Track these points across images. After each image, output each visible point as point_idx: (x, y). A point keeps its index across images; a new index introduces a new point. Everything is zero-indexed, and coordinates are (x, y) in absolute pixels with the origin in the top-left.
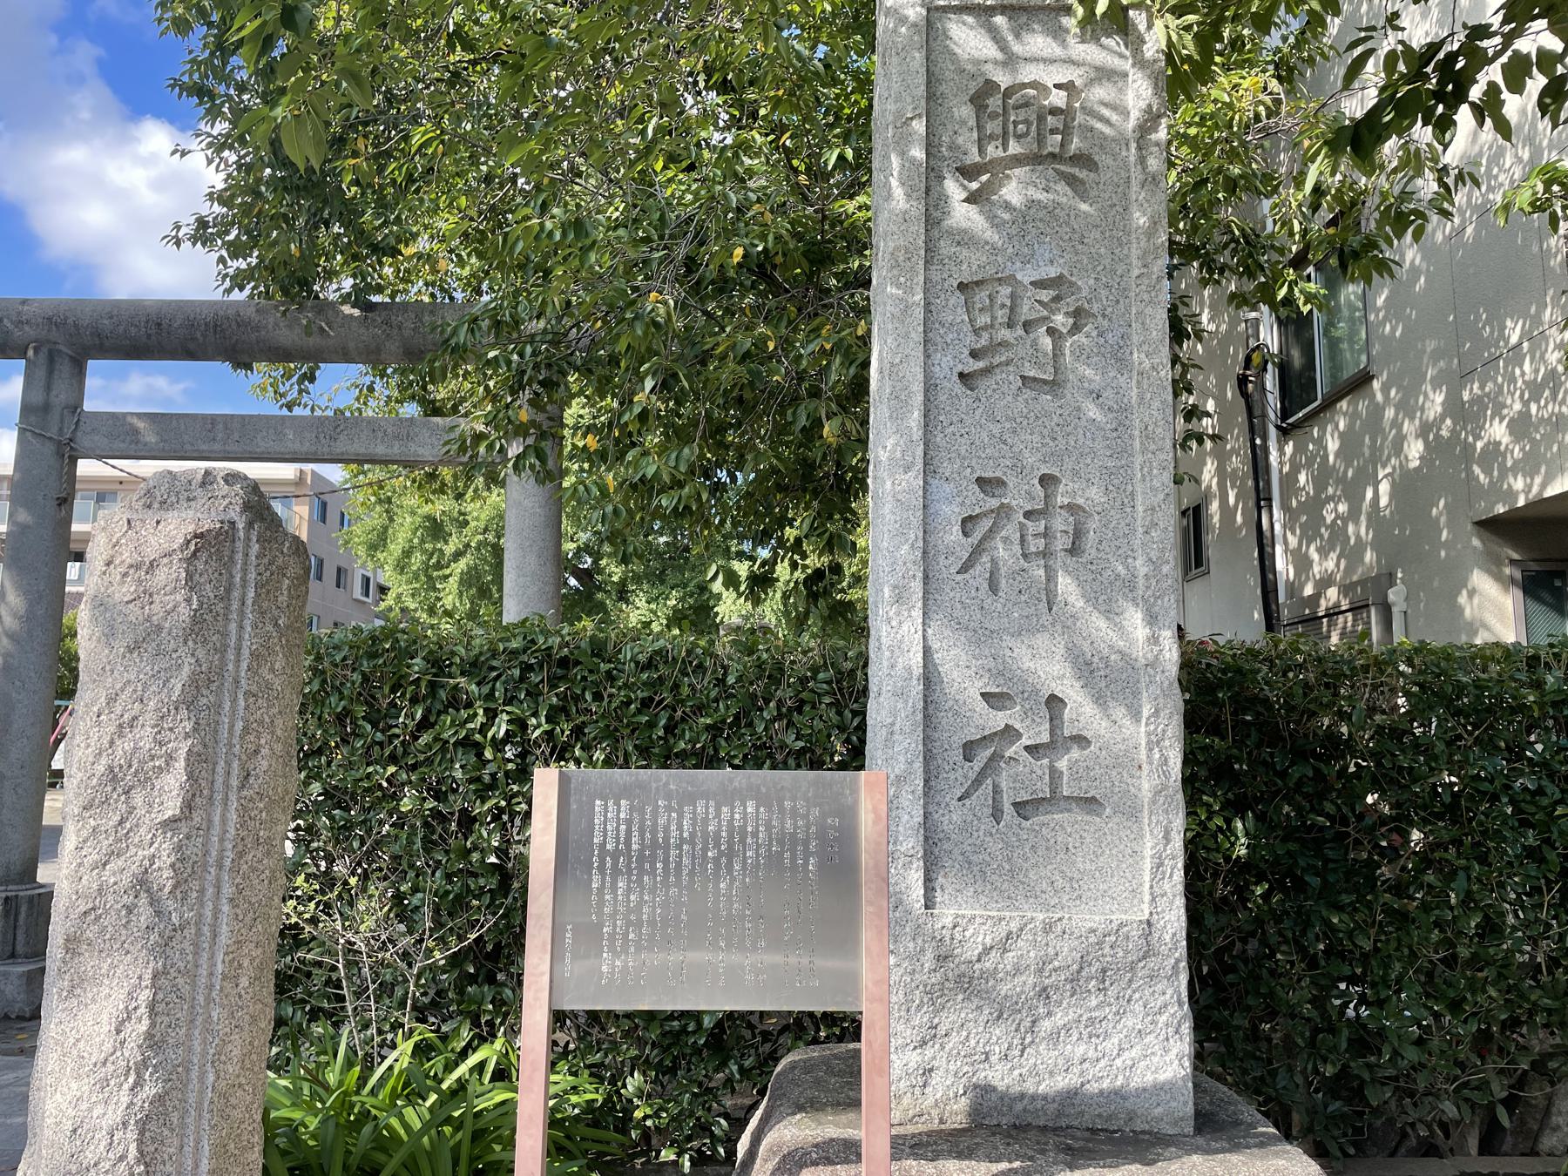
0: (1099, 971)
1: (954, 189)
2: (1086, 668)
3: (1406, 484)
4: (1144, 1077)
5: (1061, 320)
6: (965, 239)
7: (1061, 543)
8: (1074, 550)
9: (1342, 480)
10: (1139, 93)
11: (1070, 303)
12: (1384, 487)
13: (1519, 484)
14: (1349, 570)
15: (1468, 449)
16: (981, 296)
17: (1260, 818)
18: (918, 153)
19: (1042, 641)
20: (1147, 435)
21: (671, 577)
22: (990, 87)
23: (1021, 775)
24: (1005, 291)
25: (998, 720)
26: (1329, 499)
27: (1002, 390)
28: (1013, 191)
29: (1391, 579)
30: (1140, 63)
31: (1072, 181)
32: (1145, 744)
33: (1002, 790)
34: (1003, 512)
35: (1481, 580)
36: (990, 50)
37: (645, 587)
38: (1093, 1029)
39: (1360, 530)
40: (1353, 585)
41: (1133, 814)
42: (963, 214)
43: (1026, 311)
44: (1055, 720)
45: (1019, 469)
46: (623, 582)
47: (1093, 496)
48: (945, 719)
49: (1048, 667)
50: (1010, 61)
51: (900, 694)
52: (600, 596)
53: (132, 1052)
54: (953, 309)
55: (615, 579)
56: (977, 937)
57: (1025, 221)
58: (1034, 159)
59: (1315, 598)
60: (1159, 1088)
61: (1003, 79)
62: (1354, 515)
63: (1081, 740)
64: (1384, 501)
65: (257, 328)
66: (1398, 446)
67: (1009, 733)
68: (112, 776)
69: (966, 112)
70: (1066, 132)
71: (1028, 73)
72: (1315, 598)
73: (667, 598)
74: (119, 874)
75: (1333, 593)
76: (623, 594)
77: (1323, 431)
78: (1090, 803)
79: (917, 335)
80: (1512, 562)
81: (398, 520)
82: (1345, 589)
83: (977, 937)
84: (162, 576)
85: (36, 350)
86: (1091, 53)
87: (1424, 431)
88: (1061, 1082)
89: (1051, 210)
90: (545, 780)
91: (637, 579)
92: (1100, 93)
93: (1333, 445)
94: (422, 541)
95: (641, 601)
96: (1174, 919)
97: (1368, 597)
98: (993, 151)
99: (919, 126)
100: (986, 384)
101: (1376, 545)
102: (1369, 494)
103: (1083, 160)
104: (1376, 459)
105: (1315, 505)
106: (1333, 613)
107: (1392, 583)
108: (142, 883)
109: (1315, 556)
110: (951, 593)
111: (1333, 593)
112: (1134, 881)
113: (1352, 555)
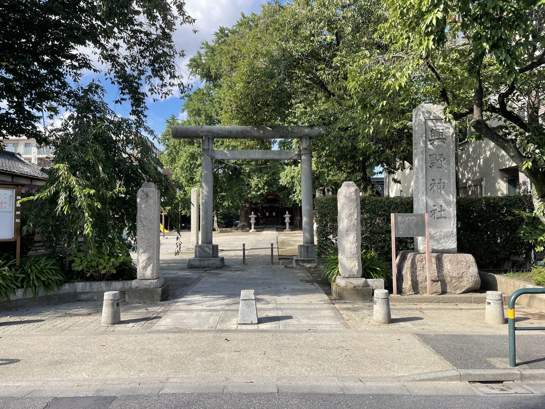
0: (447, 236)
1: (428, 143)
2: (445, 202)
3: (486, 160)
4: (451, 247)
5: (442, 159)
6: (430, 149)
7: (442, 187)
8: (443, 188)
9: (473, 158)
10: (452, 130)
11: (443, 157)
12: (482, 160)
13: (507, 163)
14: (474, 177)
15: (498, 155)
16: (432, 157)
17: (462, 222)
18: (424, 139)
19: (440, 199)
20: (453, 174)
21: (264, 171)
22: (433, 129)
23: (438, 214)
24: (435, 156)
25: (435, 208)
26: (470, 161)
27: (435, 169)
28: (436, 143)
29: (482, 180)
30: (452, 126)
31: (443, 141)
32: (452, 211)
33: (436, 214)
34: (435, 183)
35: (500, 181)
36: (433, 125)
37: (257, 174)
38: (446, 242)
39: (476, 169)
40: (474, 180)
41: (450, 219)
42: (430, 146)
43: (438, 158)
44: (441, 208)
45: (437, 178)
46: (249, 172)
47: (446, 181)
48: (428, 208)
49: (441, 202)
50: (435, 126)
51: (423, 205)
52: (242, 176)
53: (355, 241)
54: (429, 159)
55: (247, 171)
56: (433, 232)
57: (437, 147)
58: (438, 139)
59: (466, 183)
60: (453, 248)
61: (435, 129)
62: (475, 165)
63: (444, 210)
64: (481, 163)
65: (251, 132)
66: (485, 152)
67: (436, 210)
68: (350, 214)
69: (430, 133)
70: (442, 135)
71: (438, 128)
72: (466, 183)
73: (263, 177)
74: (352, 224)
75: (470, 182)
76: (249, 176)
77: (469, 147)
78: (445, 217)
79: (424, 161)
80: (506, 177)
81: (180, 153)
82: (473, 181)
83: (433, 232)
84: (352, 194)
85: (205, 137)
86: (445, 125)
87: (490, 150)
88: (442, 248)
89: (441, 146)
90: (392, 215)
91: (254, 171)
92: (447, 130)
93: (471, 150)
94: (189, 161)
95: (255, 179)
96: (455, 230)
97: (478, 183)
98: (433, 138)
99: (424, 135)
100: (433, 168)
101: (480, 172)
102: (478, 161)
103: (445, 139)
104: (480, 154)
105: (466, 162)
106: (470, 186)
107: (483, 181)
108: (354, 225)
109: (466, 174)
110: (429, 194)
111: (470, 182)
112: (451, 226)
113: (474, 174)
